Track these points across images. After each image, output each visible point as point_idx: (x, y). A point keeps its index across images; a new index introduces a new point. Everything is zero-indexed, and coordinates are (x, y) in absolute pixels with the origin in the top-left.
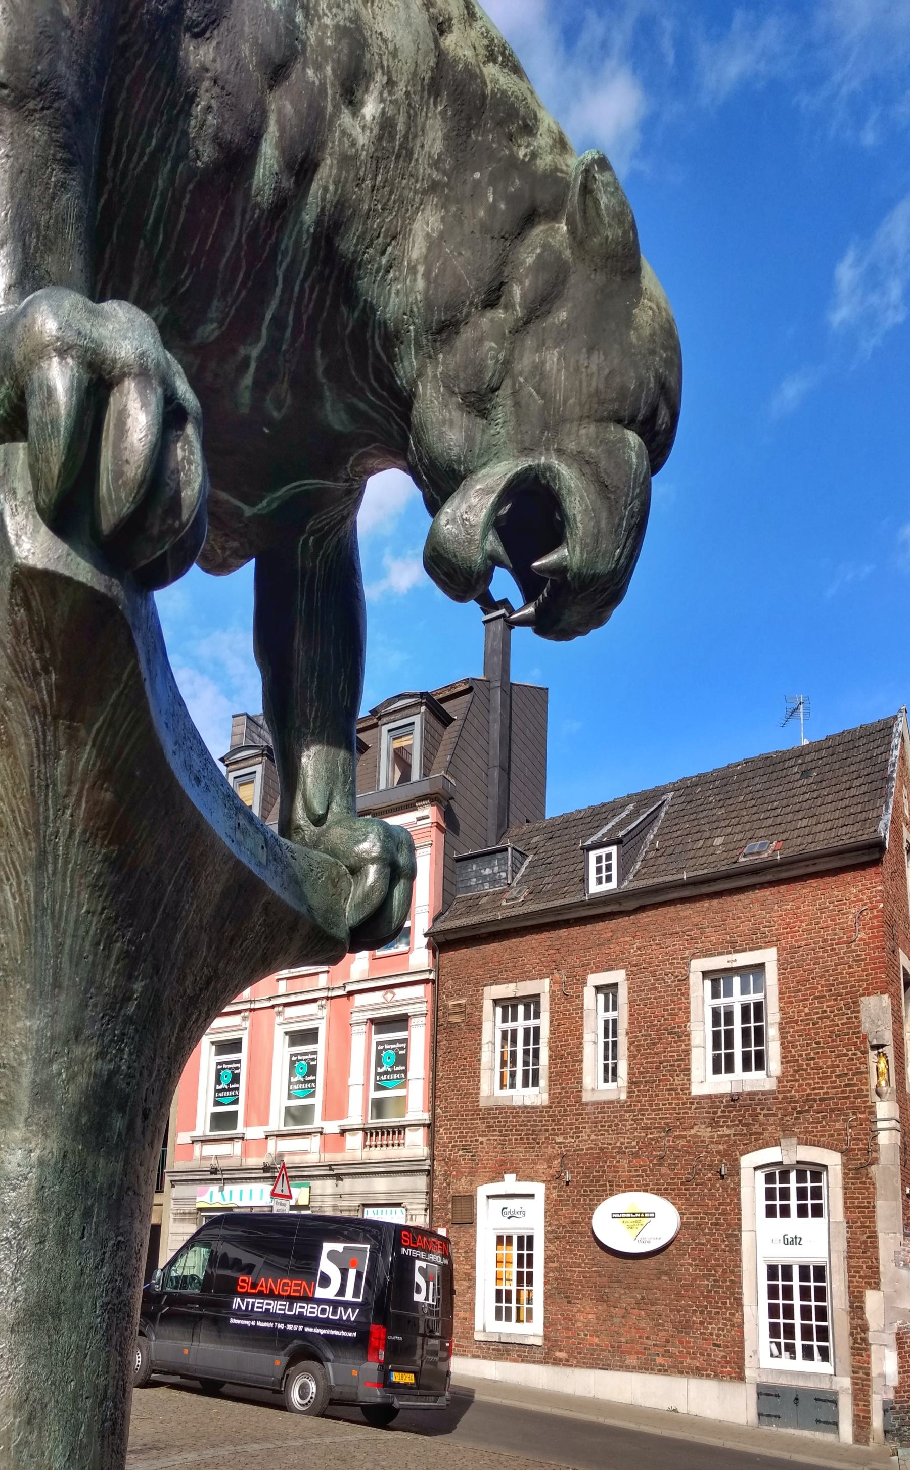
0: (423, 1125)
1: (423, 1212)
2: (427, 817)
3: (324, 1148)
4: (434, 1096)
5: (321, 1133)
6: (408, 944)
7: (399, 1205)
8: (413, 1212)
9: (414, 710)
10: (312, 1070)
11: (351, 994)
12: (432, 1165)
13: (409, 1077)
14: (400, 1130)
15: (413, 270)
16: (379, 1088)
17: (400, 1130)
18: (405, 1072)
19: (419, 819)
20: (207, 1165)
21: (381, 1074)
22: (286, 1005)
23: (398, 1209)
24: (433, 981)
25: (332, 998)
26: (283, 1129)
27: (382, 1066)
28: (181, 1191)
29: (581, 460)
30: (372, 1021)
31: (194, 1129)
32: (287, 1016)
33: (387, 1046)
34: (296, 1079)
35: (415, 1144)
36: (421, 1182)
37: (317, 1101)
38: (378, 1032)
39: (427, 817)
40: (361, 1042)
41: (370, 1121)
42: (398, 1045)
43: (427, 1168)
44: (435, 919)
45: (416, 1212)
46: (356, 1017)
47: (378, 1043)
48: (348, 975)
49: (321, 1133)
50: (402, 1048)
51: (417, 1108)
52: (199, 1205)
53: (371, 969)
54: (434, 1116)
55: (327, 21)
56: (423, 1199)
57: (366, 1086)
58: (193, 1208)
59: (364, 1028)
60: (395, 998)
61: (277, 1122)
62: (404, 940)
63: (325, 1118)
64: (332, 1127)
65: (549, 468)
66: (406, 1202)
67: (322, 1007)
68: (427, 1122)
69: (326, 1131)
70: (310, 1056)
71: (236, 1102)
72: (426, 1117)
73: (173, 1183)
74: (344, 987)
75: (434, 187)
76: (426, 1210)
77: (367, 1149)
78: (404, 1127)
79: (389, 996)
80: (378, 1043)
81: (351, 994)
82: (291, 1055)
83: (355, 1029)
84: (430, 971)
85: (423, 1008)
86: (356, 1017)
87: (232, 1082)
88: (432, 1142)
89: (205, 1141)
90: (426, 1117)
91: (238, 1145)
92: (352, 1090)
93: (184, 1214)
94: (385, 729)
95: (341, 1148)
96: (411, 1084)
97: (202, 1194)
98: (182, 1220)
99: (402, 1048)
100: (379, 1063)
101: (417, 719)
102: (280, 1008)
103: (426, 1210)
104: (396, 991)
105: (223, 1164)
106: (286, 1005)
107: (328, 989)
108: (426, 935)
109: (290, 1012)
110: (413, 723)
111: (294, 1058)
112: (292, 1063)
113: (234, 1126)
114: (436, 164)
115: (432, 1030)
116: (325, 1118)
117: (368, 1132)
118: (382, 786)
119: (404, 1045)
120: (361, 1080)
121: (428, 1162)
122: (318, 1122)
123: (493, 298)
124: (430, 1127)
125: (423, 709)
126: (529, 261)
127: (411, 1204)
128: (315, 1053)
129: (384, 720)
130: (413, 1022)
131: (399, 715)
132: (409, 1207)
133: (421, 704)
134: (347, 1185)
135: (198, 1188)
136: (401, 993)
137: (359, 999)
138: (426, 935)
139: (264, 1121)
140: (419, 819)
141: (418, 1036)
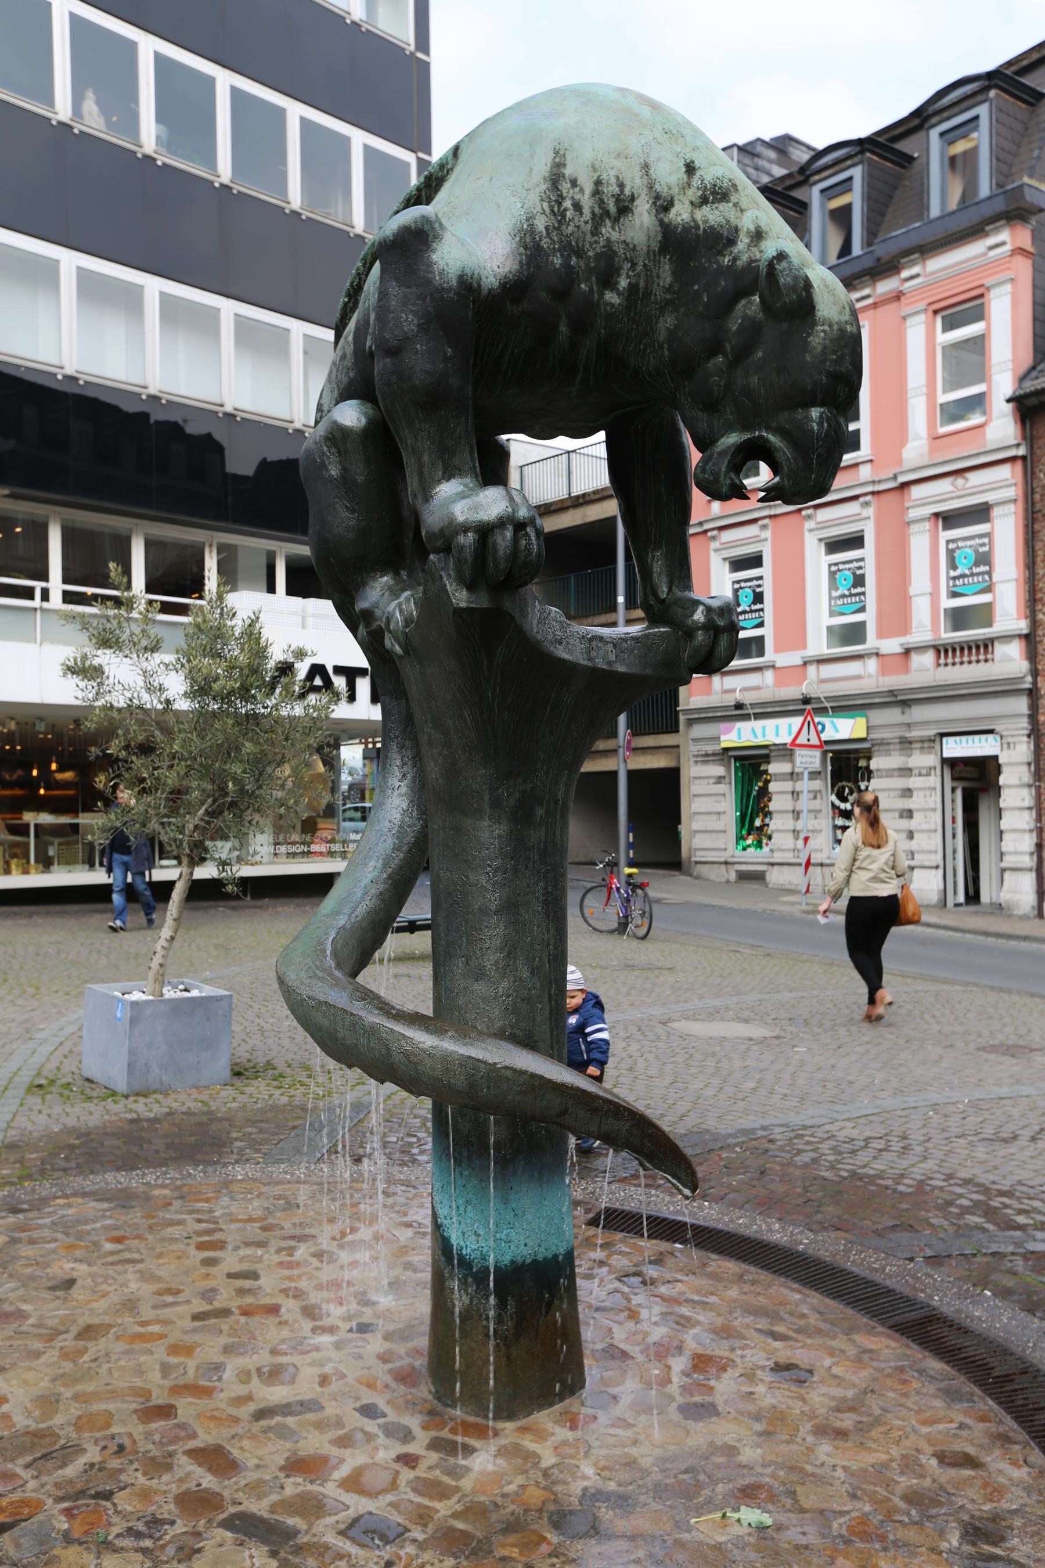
0: (1020, 636)
1: (1025, 739)
2: (1003, 243)
3: (883, 671)
4: (1032, 600)
5: (877, 654)
6: (984, 413)
7: (991, 732)
8: (1010, 740)
9: (979, 98)
10: (859, 581)
11: (905, 486)
12: (1035, 683)
13: (995, 579)
14: (985, 646)
15: (661, 346)
16: (955, 595)
17: (985, 646)
18: (989, 573)
19: (991, 248)
20: (730, 700)
21: (954, 578)
22: (721, 528)
23: (990, 737)
24: (1024, 458)
25: (879, 493)
26: (825, 651)
27: (837, 589)
28: (700, 731)
29: (780, 431)
30: (936, 515)
31: (805, 647)
32: (723, 540)
33: (841, 567)
34: (839, 593)
35: (1010, 660)
36: (1022, 705)
37: (869, 617)
38: (946, 528)
39: (1003, 243)
40: (817, 562)
41: (944, 635)
42: (978, 541)
43: (1027, 686)
44: (1022, 379)
45: (1016, 739)
46: (913, 514)
47: (948, 542)
48: (900, 461)
49: (773, 667)
50: (984, 545)
51: (1009, 613)
52: (724, 745)
53: (932, 450)
54: (1034, 623)
55: (590, 254)
56: (1024, 723)
57: (934, 595)
58: (717, 748)
59: (927, 525)
60: (968, 485)
61: (818, 644)
62: (978, 410)
63: (881, 635)
64: (892, 646)
65: (761, 437)
66: (998, 728)
67: (867, 504)
68: (1025, 631)
69: (778, 665)
70: (856, 564)
71: (761, 625)
72: (1022, 626)
73: (691, 722)
74: (895, 477)
75: (669, 302)
76: (1029, 736)
77: (942, 668)
78: (992, 640)
79: (960, 482)
80: (948, 542)
81: (905, 486)
82: (830, 565)
83: (914, 528)
84: (1018, 445)
85: (1011, 493)
86: (913, 514)
87: (754, 603)
88: (1032, 655)
89: (821, 661)
90: (1022, 626)
91: (769, 675)
92: (916, 601)
93: (707, 755)
94: (934, 134)
95: (906, 670)
96: (999, 588)
97: (727, 732)
98: (705, 762)
99: (984, 545)
100: (952, 565)
101: (983, 111)
102: (715, 533)
103: (1029, 736)
104: (970, 475)
105: (748, 698)
106: (721, 528)
107: (873, 482)
108: (1008, 401)
109: (727, 536)
110: (850, 179)
111: (834, 568)
112: (832, 575)
113: (761, 653)
114: (669, 290)
115: (1026, 518)
116: (881, 635)
117: (943, 651)
118: (935, 211)
119: (986, 540)
120: (928, 587)
121: (1029, 679)
122: (872, 641)
123: (714, 348)
124: (1030, 639)
125: (992, 93)
126: (734, 328)
127: (1007, 729)
128: (761, 578)
129: (934, 120)
130: (996, 512)
131: (956, 109)
132: (1004, 733)
133: (987, 89)
134: (918, 713)
135: (723, 726)
136: (976, 479)
137: (916, 492)
138: (1008, 401)
139: (802, 643)
140: (991, 248)
141: (1006, 531)
